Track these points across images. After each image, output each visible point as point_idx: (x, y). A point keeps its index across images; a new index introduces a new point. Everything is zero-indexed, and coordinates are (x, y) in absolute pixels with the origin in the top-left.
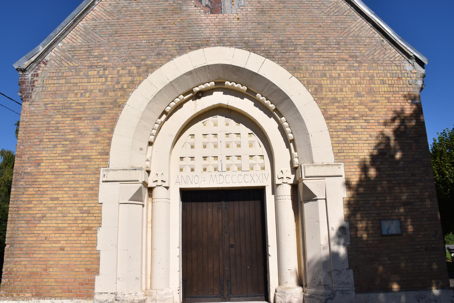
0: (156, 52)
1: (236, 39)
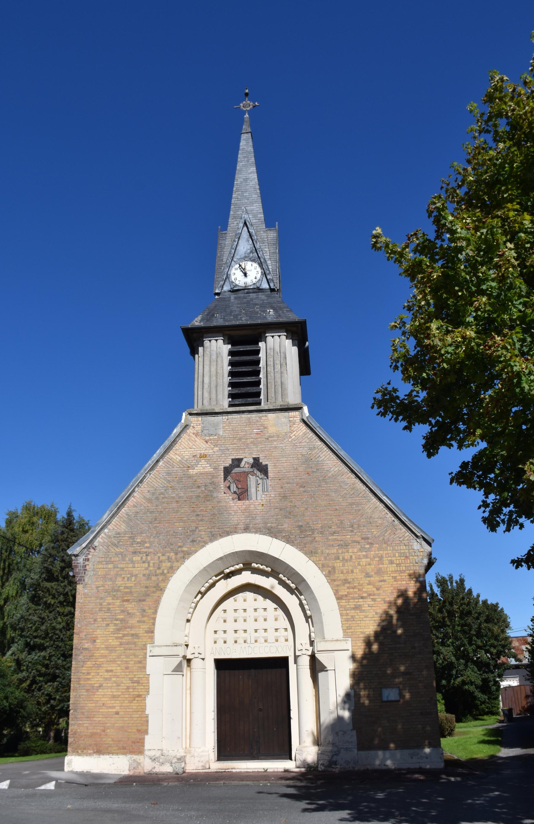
0: (191, 539)
1: (260, 525)
